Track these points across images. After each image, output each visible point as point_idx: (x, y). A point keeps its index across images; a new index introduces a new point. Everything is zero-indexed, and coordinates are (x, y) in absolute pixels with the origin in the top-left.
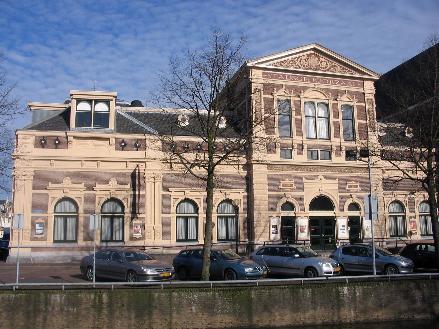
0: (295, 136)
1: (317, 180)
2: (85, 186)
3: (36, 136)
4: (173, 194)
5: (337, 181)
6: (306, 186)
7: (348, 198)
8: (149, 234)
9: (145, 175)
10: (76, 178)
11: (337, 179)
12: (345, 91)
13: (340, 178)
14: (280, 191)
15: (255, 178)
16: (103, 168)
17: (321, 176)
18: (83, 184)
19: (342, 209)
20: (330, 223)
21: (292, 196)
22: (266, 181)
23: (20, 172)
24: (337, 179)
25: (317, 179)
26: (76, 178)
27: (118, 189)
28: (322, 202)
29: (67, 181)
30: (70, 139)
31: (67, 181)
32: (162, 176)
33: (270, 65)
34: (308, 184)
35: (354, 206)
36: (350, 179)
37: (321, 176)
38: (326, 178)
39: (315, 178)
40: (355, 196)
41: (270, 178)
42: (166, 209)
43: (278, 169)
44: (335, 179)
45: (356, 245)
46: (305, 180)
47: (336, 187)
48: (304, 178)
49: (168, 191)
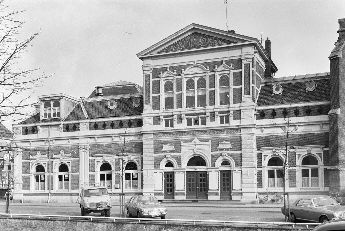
0: (232, 105)
1: (193, 143)
2: (72, 155)
3: (23, 127)
4: (263, 152)
5: (210, 142)
6: (183, 148)
7: (161, 158)
8: (82, 185)
9: (79, 147)
10: (43, 151)
11: (210, 141)
12: (222, 61)
13: (213, 140)
14: (217, 151)
15: (145, 145)
16: (266, 133)
17: (196, 140)
18: (71, 153)
19: (213, 165)
20: (205, 175)
21: (172, 157)
22: (153, 146)
23: (86, 146)
24: (210, 141)
25: (193, 142)
26: (43, 151)
27: (40, 158)
28: (197, 160)
29: (39, 153)
30: (39, 127)
31: (39, 153)
32: (89, 147)
33: (157, 53)
34: (185, 147)
35: (226, 163)
36: (221, 140)
37: (196, 140)
38: (200, 140)
39: (191, 141)
40: (170, 156)
41: (156, 143)
42: (92, 168)
43: (220, 133)
44: (208, 141)
45: (175, 194)
46: (183, 143)
47: (209, 147)
48: (182, 142)
49: (93, 156)
